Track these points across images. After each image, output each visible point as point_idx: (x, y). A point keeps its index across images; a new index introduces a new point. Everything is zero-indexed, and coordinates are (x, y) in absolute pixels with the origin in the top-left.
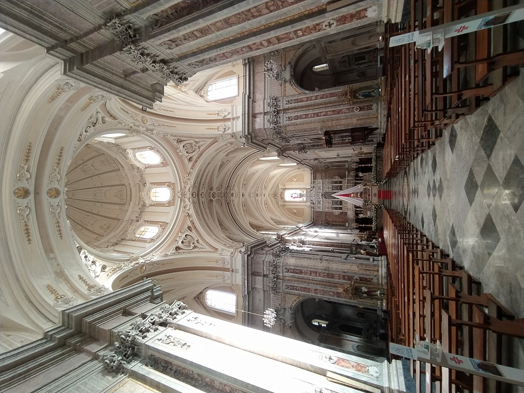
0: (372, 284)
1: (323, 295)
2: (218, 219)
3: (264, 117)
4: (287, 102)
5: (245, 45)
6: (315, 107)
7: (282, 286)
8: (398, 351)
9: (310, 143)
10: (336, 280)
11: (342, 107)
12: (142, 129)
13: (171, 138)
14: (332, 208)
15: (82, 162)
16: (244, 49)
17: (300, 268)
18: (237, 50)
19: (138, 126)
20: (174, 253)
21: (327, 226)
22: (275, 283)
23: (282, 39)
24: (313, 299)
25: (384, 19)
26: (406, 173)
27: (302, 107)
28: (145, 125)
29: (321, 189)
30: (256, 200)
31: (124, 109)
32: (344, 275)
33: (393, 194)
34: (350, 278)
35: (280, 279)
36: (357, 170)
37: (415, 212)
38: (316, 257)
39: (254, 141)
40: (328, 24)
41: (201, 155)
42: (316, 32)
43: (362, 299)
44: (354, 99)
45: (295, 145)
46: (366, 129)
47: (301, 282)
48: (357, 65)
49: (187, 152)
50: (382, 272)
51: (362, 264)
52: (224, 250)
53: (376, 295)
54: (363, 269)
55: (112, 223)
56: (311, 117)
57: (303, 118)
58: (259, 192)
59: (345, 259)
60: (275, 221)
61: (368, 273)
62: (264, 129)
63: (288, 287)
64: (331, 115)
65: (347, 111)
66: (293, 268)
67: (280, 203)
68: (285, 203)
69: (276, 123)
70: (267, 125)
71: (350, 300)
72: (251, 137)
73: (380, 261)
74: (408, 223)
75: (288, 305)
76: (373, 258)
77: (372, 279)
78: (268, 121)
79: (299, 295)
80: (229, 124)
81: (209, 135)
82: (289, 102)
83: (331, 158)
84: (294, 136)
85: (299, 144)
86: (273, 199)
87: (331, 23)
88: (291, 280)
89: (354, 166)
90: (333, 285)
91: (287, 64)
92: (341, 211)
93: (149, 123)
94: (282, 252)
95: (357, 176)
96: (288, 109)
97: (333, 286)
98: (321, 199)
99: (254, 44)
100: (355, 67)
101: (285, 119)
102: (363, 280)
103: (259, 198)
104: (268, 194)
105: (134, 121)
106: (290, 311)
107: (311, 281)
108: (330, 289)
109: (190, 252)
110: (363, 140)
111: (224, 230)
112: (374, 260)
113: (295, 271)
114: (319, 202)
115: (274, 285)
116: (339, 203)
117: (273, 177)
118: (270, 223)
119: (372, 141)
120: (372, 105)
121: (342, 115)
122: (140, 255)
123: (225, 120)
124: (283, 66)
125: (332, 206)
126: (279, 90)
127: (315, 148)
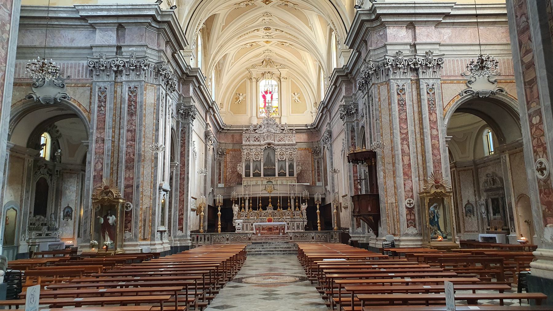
0: (121, 231)
1: (96, 154)
5: (530, 21)
6: (418, 135)
8: (31, 297)
9: (358, 124)
10: (123, 174)
11: (415, 179)
14: (248, 161)
16: (524, 19)
17: (138, 112)
18: (523, 6)
22: (107, 69)
23: (531, 88)
24: (87, 136)
25: (539, 251)
26: (302, 279)
27: (420, 113)
29: (280, 143)
30: (259, 26)
32: (132, 186)
33: (271, 258)
34: (128, 196)
35: (116, 76)
36: (311, 201)
37: (240, 295)
39: (367, 25)
40: (543, 166)
42: (534, 147)
43: (96, 216)
44: (430, 199)
47: (115, 115)
48: (487, 202)
51: (154, 214)
53: (104, 238)
54: (145, 217)
56: (401, 128)
57: (400, 114)
58: (273, 32)
60: (222, 62)
61: (140, 224)
62: (385, 46)
63: (103, 91)
64: (403, 161)
65: (408, 188)
66: (138, 100)
68: (254, 80)
70: (391, 51)
71: (90, 196)
72: (372, 21)
74: (223, 284)
75: (69, 92)
76: (165, 231)
78: (399, 53)
79: (90, 112)
83: (332, 158)
84: (370, 99)
85: (356, 105)
86: (262, 58)
87: (544, 172)
88: (115, 98)
89: (318, 196)
90: (115, 168)
91: (502, 86)
92: (244, 176)
94: (165, 80)
96: (418, 88)
97: (112, 168)
98: (262, 143)
99: (530, 39)
100: (483, 198)
102: (127, 216)
103: (262, 32)
104: (270, 48)
106: (59, 96)
107: (117, 131)
108: (107, 164)
110: (359, 212)
112: (162, 232)
113: (133, 104)
114: (257, 139)
115: (103, 66)
116: (257, 171)
117: (300, 58)
118: (217, 54)
120: (415, 226)
121: (400, 180)
124: (496, 78)
125: (252, 160)
126: (454, 71)
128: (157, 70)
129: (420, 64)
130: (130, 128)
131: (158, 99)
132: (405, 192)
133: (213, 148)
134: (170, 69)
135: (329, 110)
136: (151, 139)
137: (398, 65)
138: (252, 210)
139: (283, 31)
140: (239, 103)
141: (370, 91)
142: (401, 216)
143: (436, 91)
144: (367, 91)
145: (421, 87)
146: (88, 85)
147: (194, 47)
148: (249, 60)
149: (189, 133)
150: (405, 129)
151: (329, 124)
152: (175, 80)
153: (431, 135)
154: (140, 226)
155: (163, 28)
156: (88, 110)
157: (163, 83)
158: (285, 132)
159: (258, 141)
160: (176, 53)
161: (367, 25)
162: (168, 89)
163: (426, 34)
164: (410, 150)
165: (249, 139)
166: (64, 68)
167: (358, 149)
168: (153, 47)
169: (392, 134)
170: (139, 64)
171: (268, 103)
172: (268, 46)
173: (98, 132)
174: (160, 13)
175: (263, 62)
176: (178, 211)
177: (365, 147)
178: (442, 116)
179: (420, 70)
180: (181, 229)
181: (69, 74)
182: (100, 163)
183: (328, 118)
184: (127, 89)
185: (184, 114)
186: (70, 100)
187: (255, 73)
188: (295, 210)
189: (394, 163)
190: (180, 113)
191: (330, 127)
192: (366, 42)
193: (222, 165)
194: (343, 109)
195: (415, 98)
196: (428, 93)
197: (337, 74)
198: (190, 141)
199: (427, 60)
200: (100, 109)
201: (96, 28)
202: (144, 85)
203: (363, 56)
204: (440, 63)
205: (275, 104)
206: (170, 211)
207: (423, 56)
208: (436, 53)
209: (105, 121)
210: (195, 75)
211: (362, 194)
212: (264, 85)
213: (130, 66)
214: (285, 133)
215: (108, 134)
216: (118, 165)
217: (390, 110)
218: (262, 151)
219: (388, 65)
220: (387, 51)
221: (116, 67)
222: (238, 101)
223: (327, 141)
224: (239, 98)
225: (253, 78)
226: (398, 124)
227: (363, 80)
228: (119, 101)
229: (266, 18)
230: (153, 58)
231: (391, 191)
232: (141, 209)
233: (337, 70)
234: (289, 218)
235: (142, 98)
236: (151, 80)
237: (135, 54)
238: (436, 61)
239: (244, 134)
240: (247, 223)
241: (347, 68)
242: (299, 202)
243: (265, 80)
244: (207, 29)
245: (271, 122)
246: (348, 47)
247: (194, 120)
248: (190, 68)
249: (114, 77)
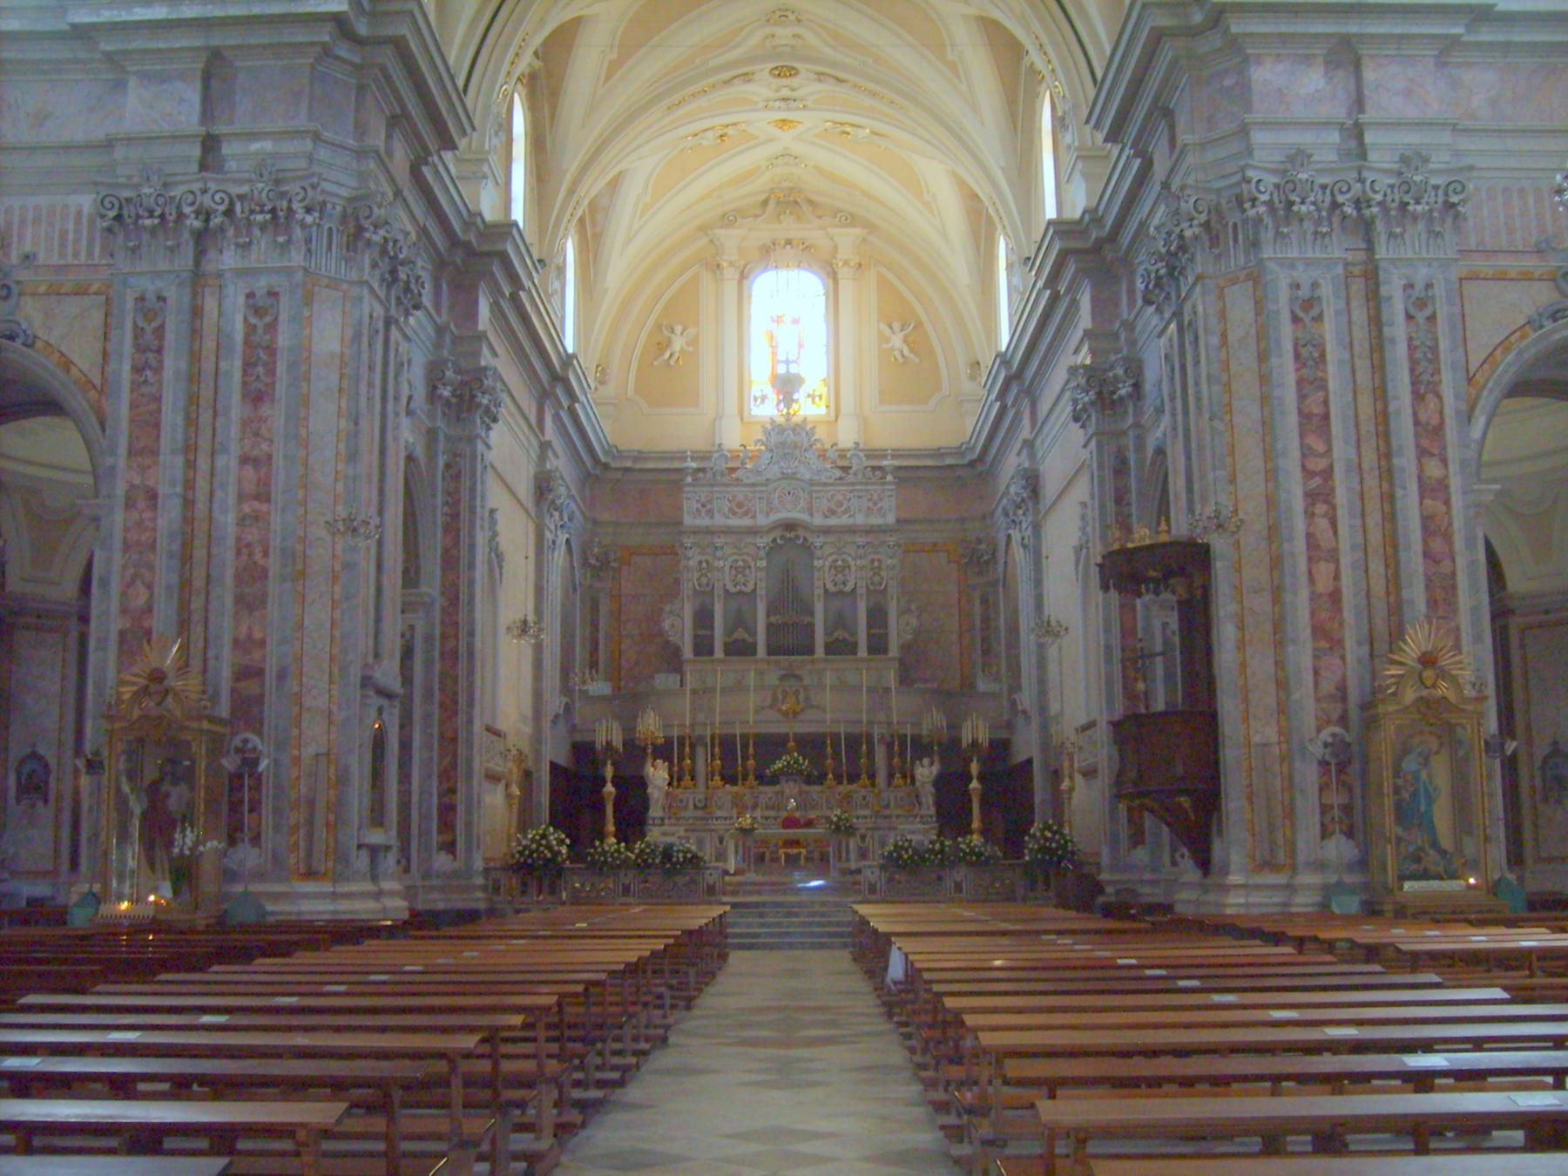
1: (127, 546)
3: (1327, 124)
4: (1419, 285)
6: (1372, 482)
9: (1140, 446)
17: (281, 390)
21: (585, 563)
27: (1381, 393)
29: (833, 521)
34: (248, 711)
38: (368, 493)
39: (1167, 52)
45: (1132, 343)
46: (1209, 799)
50: (306, 896)
51: (342, 780)
56: (1306, 453)
57: (1302, 397)
59: (366, 682)
64: (1312, 580)
65: (1327, 687)
66: (283, 340)
67: (730, 238)
69: (1285, 211)
72: (1192, 33)
73: (369, 887)
76: (387, 848)
77: (256, 840)
82: (1420, 302)
84: (1188, 338)
85: (1135, 370)
92: (688, 652)
94: (385, 265)
95: (921, 748)
96: (1374, 298)
98: (762, 521)
101: (1304, 276)
107: (203, 464)
112: (374, 851)
116: (740, 634)
119: (1137, 839)
121: (1302, 655)
125: (719, 592)
126: (1511, 232)
127: (1108, 474)
129: (1380, 204)
132: (1318, 700)
133: (568, 540)
134: (404, 222)
138: (720, 783)
140: (672, 363)
141: (1187, 308)
142: (1298, 796)
143: (1443, 311)
145: (1384, 290)
146: (95, 288)
147: (495, 141)
149: (473, 475)
151: (1029, 444)
152: (423, 267)
153: (1420, 478)
154: (292, 822)
157: (377, 277)
158: (850, 478)
159: (746, 513)
160: (427, 163)
162: (393, 302)
165: (709, 507)
167: (1142, 536)
168: (338, 139)
169: (1272, 474)
170: (285, 204)
172: (786, 139)
175: (765, 203)
176: (435, 777)
177: (1169, 525)
178: (1464, 407)
179: (1380, 226)
180: (450, 847)
181: (28, 248)
182: (143, 582)
183: (1026, 421)
184: (241, 300)
188: (889, 784)
189: (1278, 588)
191: (1032, 456)
192: (1169, 114)
193: (604, 609)
194: (1083, 381)
195: (1361, 334)
196: (1409, 317)
198: (478, 509)
199: (1405, 187)
200: (143, 379)
201: (129, 69)
203: (1160, 169)
204: (1454, 199)
206: (405, 777)
207: (1274, 172)
208: (1440, 160)
210: (499, 247)
211: (1153, 710)
213: (252, 212)
214: (852, 484)
215: (168, 473)
216: (208, 593)
218: (762, 553)
219: (1257, 203)
220: (1249, 151)
222: (667, 355)
223: (1020, 512)
224: (669, 343)
225: (725, 264)
226: (1295, 434)
227: (1160, 265)
231: (1266, 697)
232: (297, 760)
233: (1060, 228)
234: (866, 817)
237: (273, 165)
238: (1440, 193)
239: (689, 485)
240: (703, 834)
242: (902, 754)
246: (1100, 137)
247: (492, 425)
248: (479, 221)
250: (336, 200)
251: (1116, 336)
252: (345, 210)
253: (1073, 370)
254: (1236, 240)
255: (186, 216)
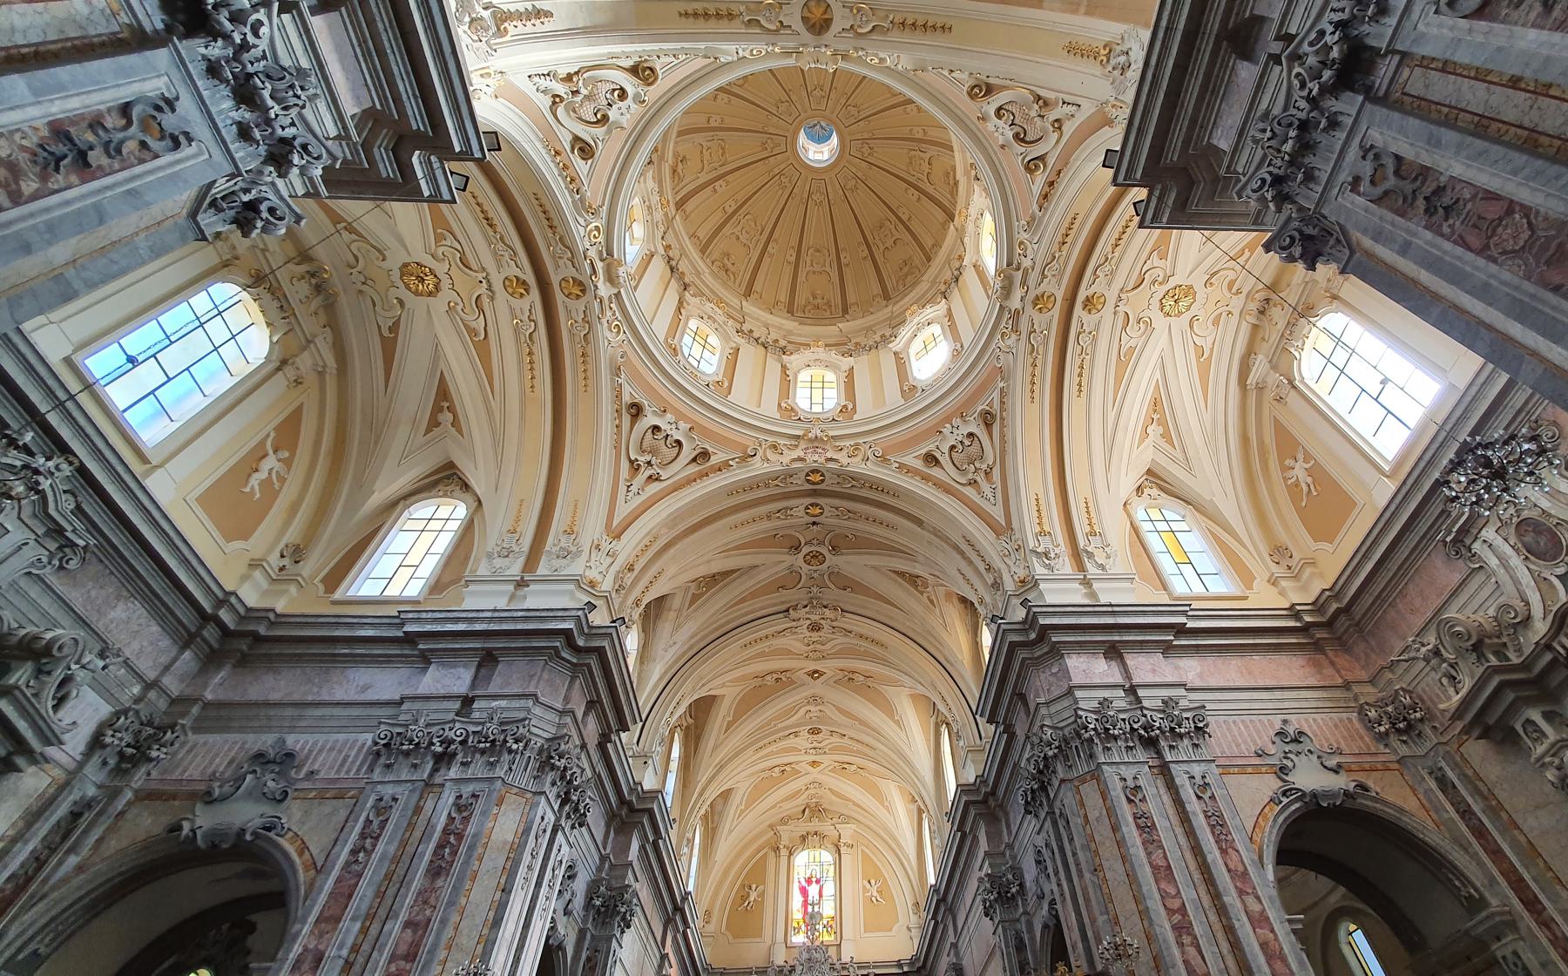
2: (733, 571)
4: (1198, 780)
7: (397, 784)
9: (1030, 925)
12: (1015, 303)
13: (996, 395)
15: (904, 218)
17: (457, 866)
19: (1024, 283)
20: (619, 396)
28: (1029, 307)
31: (1075, 227)
35: (435, 770)
39: (1022, 654)
41: (948, 490)
45: (1014, 857)
47: (389, 877)
49: (953, 447)
52: (609, 560)
55: (738, 281)
56: (1164, 896)
57: (1149, 854)
62: (1070, 691)
66: (471, 829)
68: (784, 852)
70: (1087, 701)
72: (1033, 644)
78: (1105, 703)
79: (320, 870)
80: (1066, 566)
81: (1019, 503)
84: (1061, 824)
85: (1017, 872)
86: (801, 800)
88: (411, 826)
91: (1361, 777)
93: (1037, 317)
103: (803, 741)
104: (821, 778)
105: (1038, 269)
109: (617, 447)
111: (692, 591)
113: (452, 836)
117: (880, 797)
122: (622, 290)
123: (1077, 556)
126: (1238, 746)
128: (545, 755)
130: (418, 914)
131: (527, 831)
135: (950, 909)
136: (467, 954)
137: (1109, 729)
139: (850, 632)
144: (1046, 809)
148: (775, 806)
150: (1173, 897)
151: (955, 946)
155: (584, 665)
156: (319, 865)
160: (610, 742)
161: (1022, 654)
162: (564, 815)
163: (1150, 667)
164: (1209, 966)
166: (310, 751)
169: (1144, 913)
171: (813, 905)
172: (815, 773)
173: (316, 932)
174: (586, 631)
175: (804, 811)
184: (451, 800)
185: (603, 909)
186: (282, 836)
187: (787, 834)
190: (594, 905)
192: (1023, 698)
194: (988, 885)
196: (1199, 798)
197: (964, 798)
202: (500, 790)
203: (1020, 732)
204: (1201, 725)
205: (828, 909)
209: (350, 896)
212: (806, 862)
213: (480, 742)
217: (1121, 843)
221: (444, 745)
226: (1152, 881)
228: (417, 834)
229: (812, 708)
230: (542, 726)
235: (482, 825)
236: (523, 779)
241: (985, 782)
243: (806, 851)
244: (696, 727)
245: (818, 955)
248: (639, 789)
249: (428, 771)
250: (538, 740)
251: (1003, 854)
252: (543, 745)
253: (981, 880)
254: (1079, 756)
255: (433, 744)
